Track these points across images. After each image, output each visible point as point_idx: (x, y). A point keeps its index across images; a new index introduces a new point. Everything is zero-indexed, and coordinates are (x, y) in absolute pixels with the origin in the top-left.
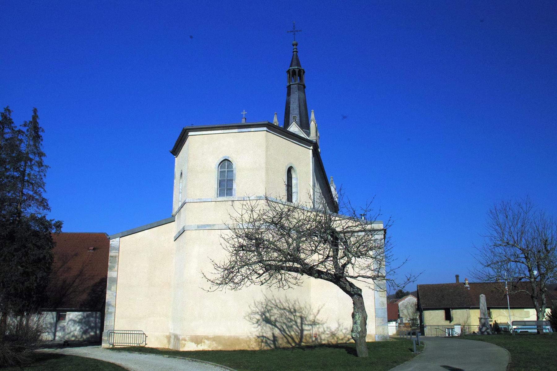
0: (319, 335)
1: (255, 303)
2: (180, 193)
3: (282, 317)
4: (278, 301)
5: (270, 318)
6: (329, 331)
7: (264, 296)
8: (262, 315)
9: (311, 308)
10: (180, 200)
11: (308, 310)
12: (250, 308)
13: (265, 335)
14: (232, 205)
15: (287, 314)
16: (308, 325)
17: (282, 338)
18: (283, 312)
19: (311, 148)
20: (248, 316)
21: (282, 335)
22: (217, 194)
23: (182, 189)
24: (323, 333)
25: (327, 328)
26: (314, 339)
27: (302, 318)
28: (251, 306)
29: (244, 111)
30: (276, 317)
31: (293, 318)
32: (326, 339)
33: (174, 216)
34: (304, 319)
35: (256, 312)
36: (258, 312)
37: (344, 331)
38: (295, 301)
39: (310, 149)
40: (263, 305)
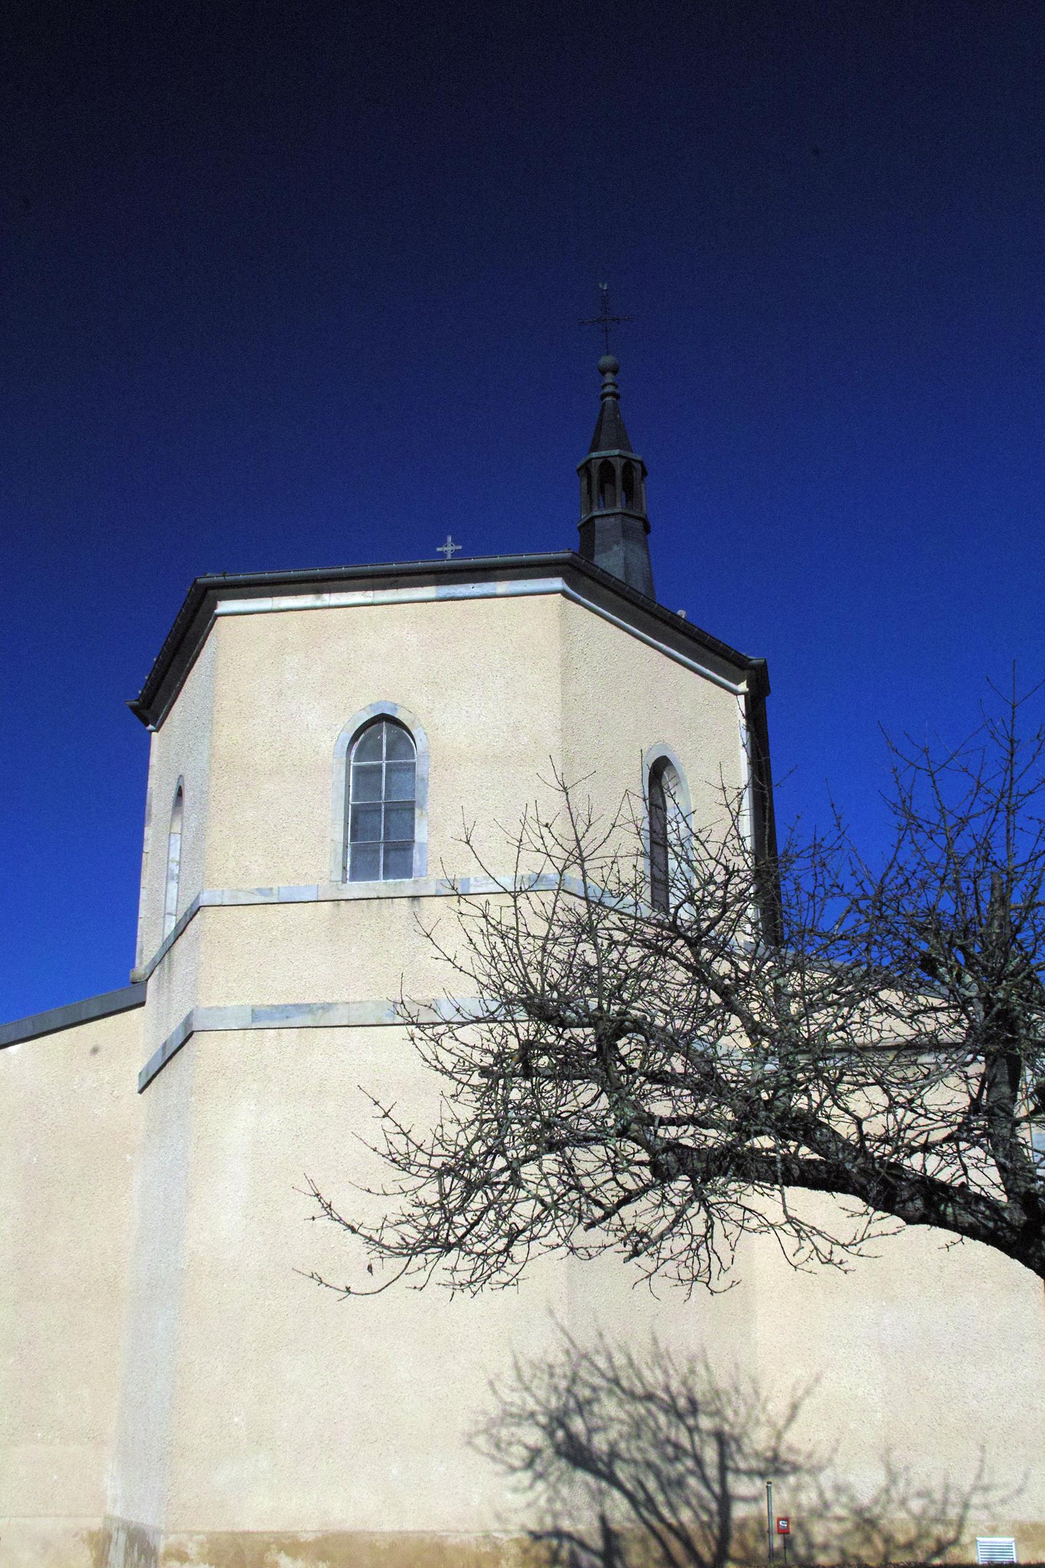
0: (800, 1525)
1: (517, 1367)
2: (169, 877)
3: (639, 1437)
4: (620, 1360)
5: (589, 1440)
6: (845, 1506)
7: (560, 1335)
8: (555, 1425)
9: (756, 1393)
10: (171, 906)
11: (746, 1404)
12: (495, 1392)
13: (566, 1525)
14: (468, 842)
15: (662, 1419)
16: (750, 1473)
17: (643, 1541)
18: (643, 1411)
19: (743, 687)
20: (486, 1431)
21: (643, 1526)
22: (344, 868)
23: (179, 863)
24: (821, 1512)
25: (838, 1489)
26: (777, 1542)
27: (721, 1439)
28: (498, 1386)
29: (450, 539)
30: (613, 1434)
31: (684, 1440)
32: (835, 1543)
33: (140, 985)
34: (733, 1447)
35: (526, 1414)
36: (532, 1415)
37: (916, 1505)
38: (692, 1360)
39: (736, 693)
40: (556, 1380)
